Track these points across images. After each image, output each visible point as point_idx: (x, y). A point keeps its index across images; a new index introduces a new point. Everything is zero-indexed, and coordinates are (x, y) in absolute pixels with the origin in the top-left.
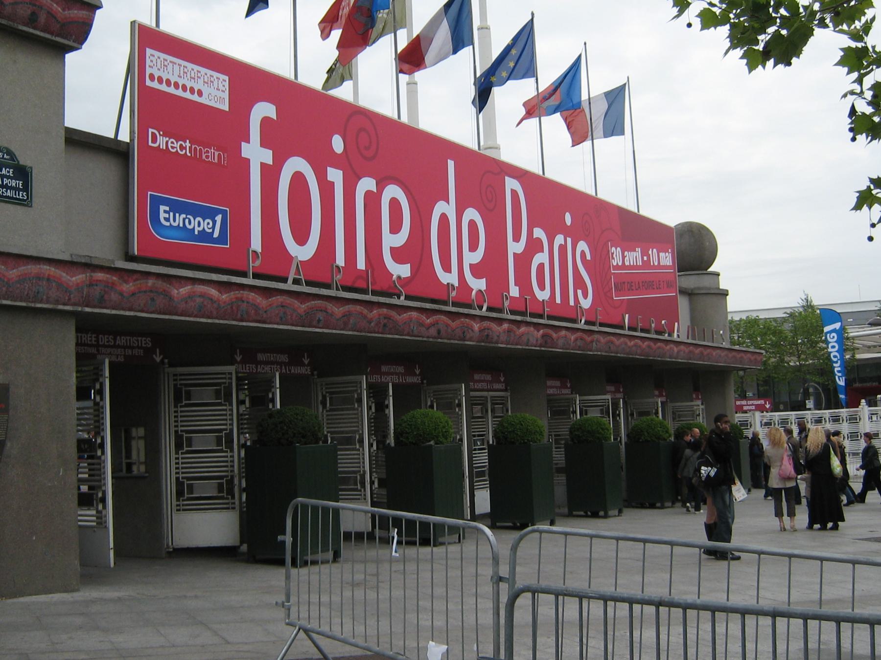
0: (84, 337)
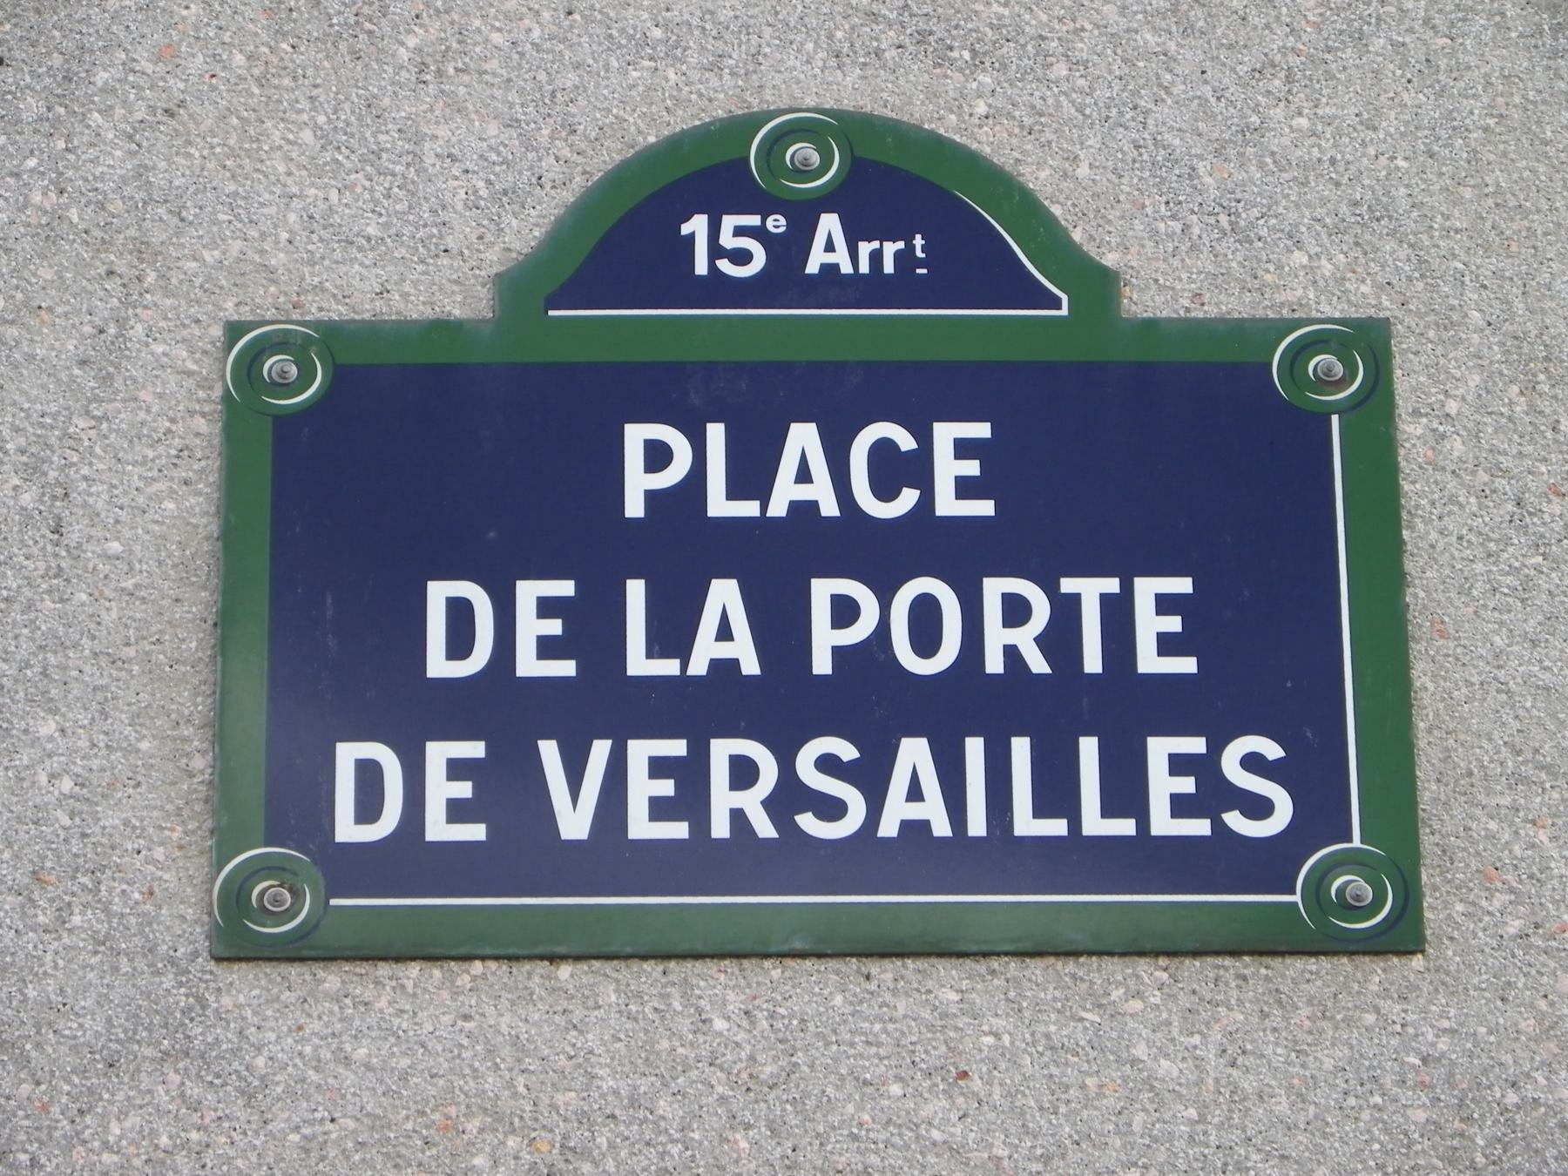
0: (744, 773)
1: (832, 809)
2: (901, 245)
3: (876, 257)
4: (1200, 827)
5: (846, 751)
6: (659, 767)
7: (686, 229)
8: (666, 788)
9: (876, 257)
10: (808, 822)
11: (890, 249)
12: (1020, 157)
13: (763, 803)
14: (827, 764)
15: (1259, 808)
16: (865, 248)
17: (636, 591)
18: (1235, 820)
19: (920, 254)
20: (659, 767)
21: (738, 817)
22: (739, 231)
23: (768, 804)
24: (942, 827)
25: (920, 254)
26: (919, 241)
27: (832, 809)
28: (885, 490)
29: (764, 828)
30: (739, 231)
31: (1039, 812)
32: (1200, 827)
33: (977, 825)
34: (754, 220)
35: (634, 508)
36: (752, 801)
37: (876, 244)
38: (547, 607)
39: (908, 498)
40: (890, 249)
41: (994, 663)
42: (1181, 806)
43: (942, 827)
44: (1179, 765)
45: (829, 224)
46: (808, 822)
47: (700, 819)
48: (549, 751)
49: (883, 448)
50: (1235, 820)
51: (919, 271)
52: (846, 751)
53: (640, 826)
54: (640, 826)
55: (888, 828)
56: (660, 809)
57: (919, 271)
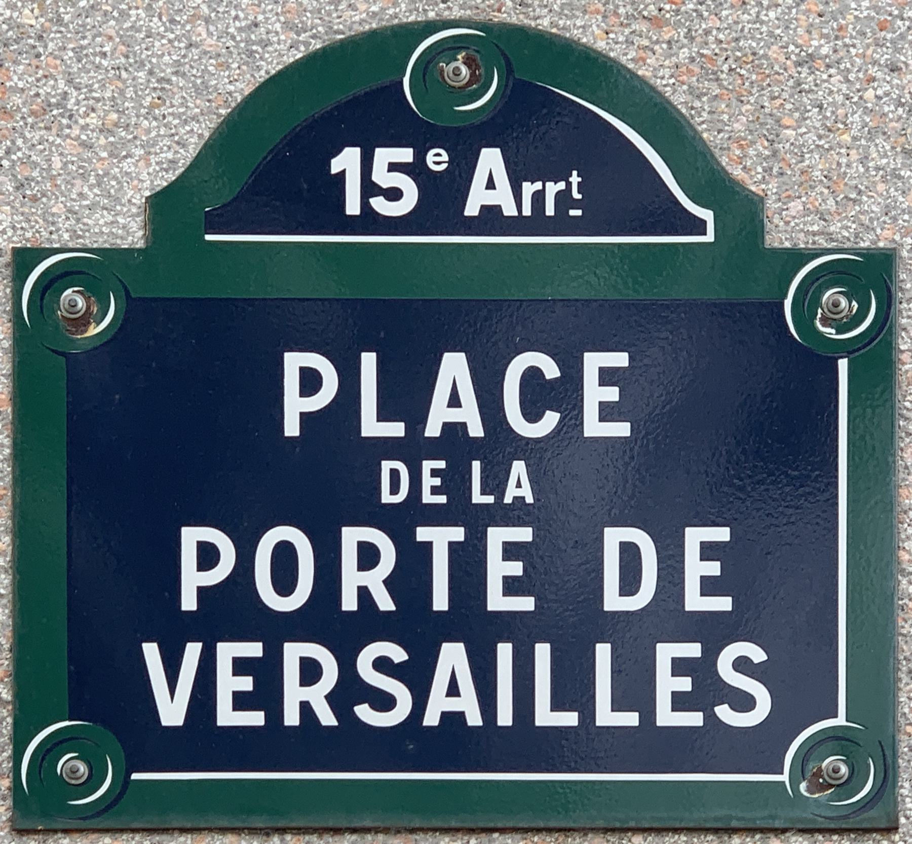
1: (385, 702)
2: (562, 185)
3: (539, 198)
4: (695, 719)
5: (398, 654)
6: (241, 666)
7: (336, 165)
8: (246, 684)
9: (539, 198)
10: (364, 712)
12: (763, 92)
13: (326, 697)
14: (382, 665)
15: (745, 703)
16: (529, 189)
17: (476, 466)
18: (724, 712)
19: (577, 196)
20: (241, 666)
21: (306, 708)
22: (394, 167)
23: (331, 698)
24: (474, 719)
25: (577, 196)
26: (575, 179)
27: (385, 702)
28: (532, 414)
29: (327, 717)
30: (394, 167)
31: (557, 705)
32: (695, 719)
33: (505, 717)
35: (292, 428)
37: (538, 185)
38: (435, 473)
39: (551, 420)
40: (552, 189)
41: (349, 603)
42: (680, 702)
43: (474, 719)
44: (680, 667)
46: (364, 712)
47: (275, 710)
48: (151, 652)
49: (532, 376)
50: (724, 712)
51: (573, 213)
52: (398, 654)
55: (431, 719)
56: (241, 701)
57: (573, 213)
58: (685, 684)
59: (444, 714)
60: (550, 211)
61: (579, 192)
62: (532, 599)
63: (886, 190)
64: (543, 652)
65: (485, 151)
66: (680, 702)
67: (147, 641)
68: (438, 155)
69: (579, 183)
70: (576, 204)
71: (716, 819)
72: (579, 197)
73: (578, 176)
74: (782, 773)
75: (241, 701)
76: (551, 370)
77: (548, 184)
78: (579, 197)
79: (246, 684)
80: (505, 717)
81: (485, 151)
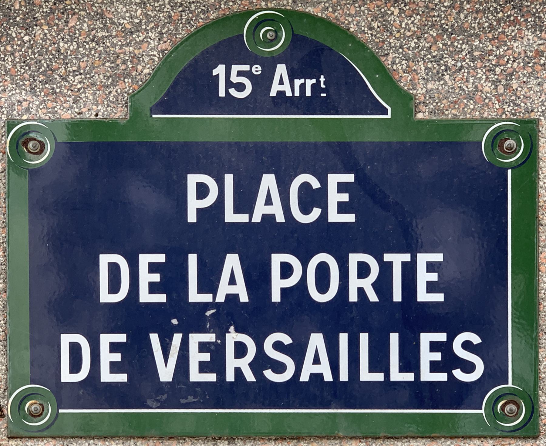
1: (279, 368)
3: (303, 87)
4: (442, 377)
5: (287, 340)
6: (203, 347)
7: (215, 72)
8: (206, 357)
9: (303, 87)
10: (269, 374)
11: (310, 83)
14: (278, 346)
15: (469, 367)
16: (298, 83)
18: (458, 374)
19: (323, 86)
20: (203, 347)
21: (238, 372)
22: (240, 74)
23: (251, 365)
24: (328, 377)
25: (323, 86)
26: (322, 79)
27: (279, 368)
29: (250, 377)
32: (442, 377)
33: (344, 376)
34: (246, 68)
35: (192, 218)
36: (244, 364)
37: (302, 81)
40: (310, 83)
42: (435, 367)
43: (328, 377)
44: (434, 346)
45: (281, 70)
46: (269, 374)
47: (221, 371)
48: (154, 338)
50: (458, 374)
52: (287, 340)
53: (195, 376)
54: (195, 376)
55: (304, 377)
56: (203, 367)
57: (323, 95)
58: (437, 356)
59: (312, 375)
60: (308, 93)
61: (324, 84)
62: (279, 300)
63: (98, 33)
64: (364, 338)
65: (279, 66)
66: (435, 367)
67: (291, 344)
68: (257, 68)
69: (324, 81)
70: (323, 91)
71: (372, 433)
72: (324, 87)
73: (324, 78)
74: (482, 409)
75: (203, 367)
76: (316, 184)
77: (307, 80)
78: (324, 87)
79: (206, 357)
80: (344, 376)
81: (279, 66)
